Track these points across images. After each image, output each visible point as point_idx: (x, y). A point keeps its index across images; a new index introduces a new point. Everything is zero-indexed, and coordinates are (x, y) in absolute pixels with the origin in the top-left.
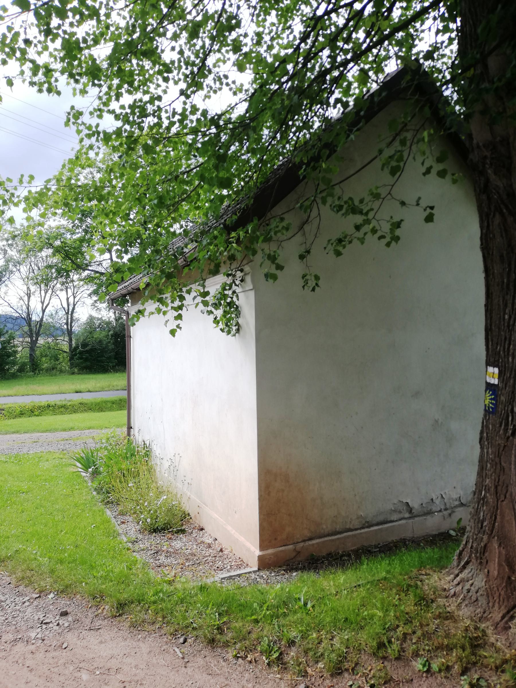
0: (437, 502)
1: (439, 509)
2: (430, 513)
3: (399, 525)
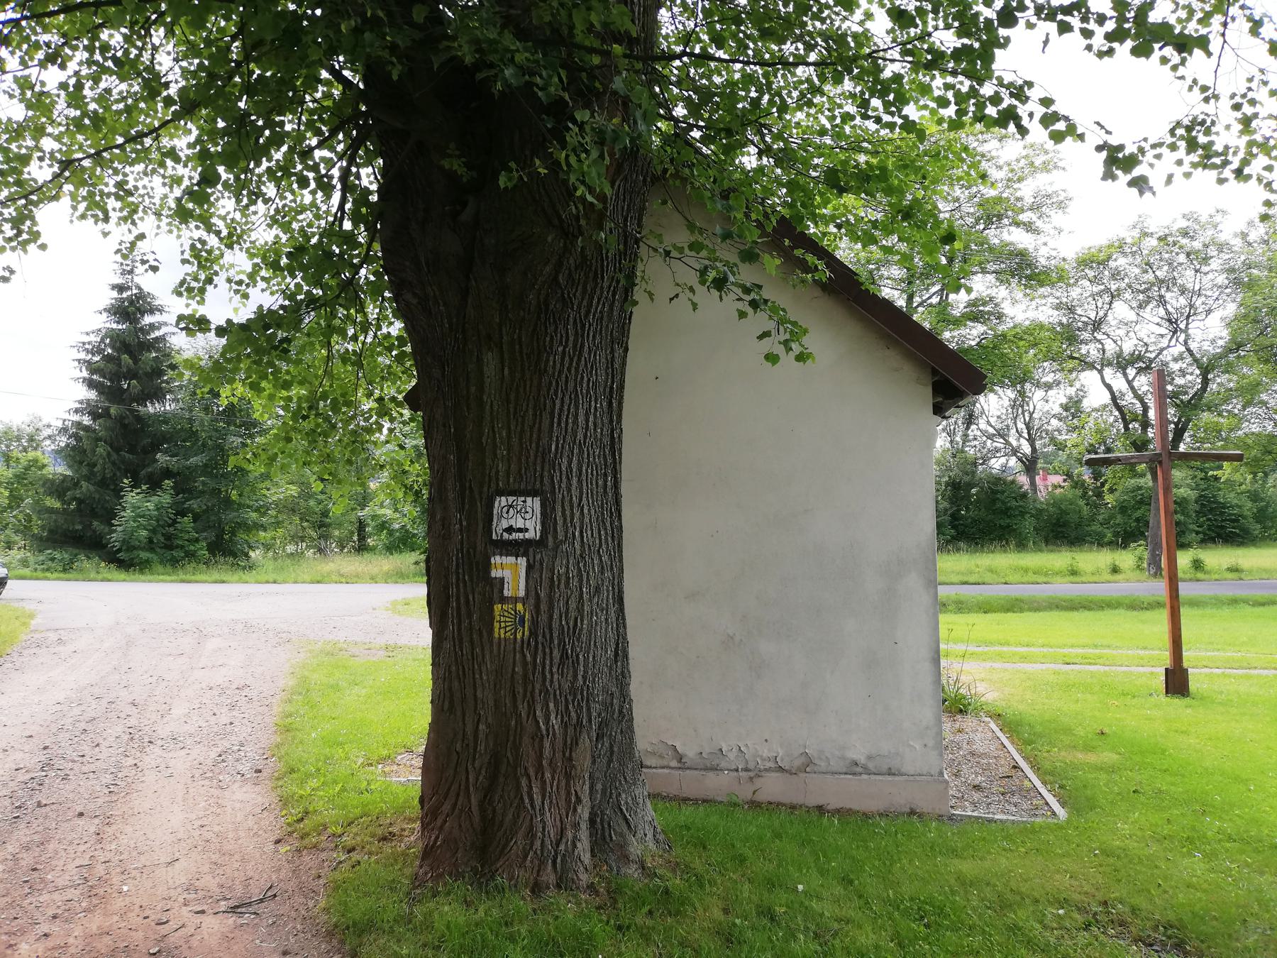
0: (732, 756)
2: (715, 769)
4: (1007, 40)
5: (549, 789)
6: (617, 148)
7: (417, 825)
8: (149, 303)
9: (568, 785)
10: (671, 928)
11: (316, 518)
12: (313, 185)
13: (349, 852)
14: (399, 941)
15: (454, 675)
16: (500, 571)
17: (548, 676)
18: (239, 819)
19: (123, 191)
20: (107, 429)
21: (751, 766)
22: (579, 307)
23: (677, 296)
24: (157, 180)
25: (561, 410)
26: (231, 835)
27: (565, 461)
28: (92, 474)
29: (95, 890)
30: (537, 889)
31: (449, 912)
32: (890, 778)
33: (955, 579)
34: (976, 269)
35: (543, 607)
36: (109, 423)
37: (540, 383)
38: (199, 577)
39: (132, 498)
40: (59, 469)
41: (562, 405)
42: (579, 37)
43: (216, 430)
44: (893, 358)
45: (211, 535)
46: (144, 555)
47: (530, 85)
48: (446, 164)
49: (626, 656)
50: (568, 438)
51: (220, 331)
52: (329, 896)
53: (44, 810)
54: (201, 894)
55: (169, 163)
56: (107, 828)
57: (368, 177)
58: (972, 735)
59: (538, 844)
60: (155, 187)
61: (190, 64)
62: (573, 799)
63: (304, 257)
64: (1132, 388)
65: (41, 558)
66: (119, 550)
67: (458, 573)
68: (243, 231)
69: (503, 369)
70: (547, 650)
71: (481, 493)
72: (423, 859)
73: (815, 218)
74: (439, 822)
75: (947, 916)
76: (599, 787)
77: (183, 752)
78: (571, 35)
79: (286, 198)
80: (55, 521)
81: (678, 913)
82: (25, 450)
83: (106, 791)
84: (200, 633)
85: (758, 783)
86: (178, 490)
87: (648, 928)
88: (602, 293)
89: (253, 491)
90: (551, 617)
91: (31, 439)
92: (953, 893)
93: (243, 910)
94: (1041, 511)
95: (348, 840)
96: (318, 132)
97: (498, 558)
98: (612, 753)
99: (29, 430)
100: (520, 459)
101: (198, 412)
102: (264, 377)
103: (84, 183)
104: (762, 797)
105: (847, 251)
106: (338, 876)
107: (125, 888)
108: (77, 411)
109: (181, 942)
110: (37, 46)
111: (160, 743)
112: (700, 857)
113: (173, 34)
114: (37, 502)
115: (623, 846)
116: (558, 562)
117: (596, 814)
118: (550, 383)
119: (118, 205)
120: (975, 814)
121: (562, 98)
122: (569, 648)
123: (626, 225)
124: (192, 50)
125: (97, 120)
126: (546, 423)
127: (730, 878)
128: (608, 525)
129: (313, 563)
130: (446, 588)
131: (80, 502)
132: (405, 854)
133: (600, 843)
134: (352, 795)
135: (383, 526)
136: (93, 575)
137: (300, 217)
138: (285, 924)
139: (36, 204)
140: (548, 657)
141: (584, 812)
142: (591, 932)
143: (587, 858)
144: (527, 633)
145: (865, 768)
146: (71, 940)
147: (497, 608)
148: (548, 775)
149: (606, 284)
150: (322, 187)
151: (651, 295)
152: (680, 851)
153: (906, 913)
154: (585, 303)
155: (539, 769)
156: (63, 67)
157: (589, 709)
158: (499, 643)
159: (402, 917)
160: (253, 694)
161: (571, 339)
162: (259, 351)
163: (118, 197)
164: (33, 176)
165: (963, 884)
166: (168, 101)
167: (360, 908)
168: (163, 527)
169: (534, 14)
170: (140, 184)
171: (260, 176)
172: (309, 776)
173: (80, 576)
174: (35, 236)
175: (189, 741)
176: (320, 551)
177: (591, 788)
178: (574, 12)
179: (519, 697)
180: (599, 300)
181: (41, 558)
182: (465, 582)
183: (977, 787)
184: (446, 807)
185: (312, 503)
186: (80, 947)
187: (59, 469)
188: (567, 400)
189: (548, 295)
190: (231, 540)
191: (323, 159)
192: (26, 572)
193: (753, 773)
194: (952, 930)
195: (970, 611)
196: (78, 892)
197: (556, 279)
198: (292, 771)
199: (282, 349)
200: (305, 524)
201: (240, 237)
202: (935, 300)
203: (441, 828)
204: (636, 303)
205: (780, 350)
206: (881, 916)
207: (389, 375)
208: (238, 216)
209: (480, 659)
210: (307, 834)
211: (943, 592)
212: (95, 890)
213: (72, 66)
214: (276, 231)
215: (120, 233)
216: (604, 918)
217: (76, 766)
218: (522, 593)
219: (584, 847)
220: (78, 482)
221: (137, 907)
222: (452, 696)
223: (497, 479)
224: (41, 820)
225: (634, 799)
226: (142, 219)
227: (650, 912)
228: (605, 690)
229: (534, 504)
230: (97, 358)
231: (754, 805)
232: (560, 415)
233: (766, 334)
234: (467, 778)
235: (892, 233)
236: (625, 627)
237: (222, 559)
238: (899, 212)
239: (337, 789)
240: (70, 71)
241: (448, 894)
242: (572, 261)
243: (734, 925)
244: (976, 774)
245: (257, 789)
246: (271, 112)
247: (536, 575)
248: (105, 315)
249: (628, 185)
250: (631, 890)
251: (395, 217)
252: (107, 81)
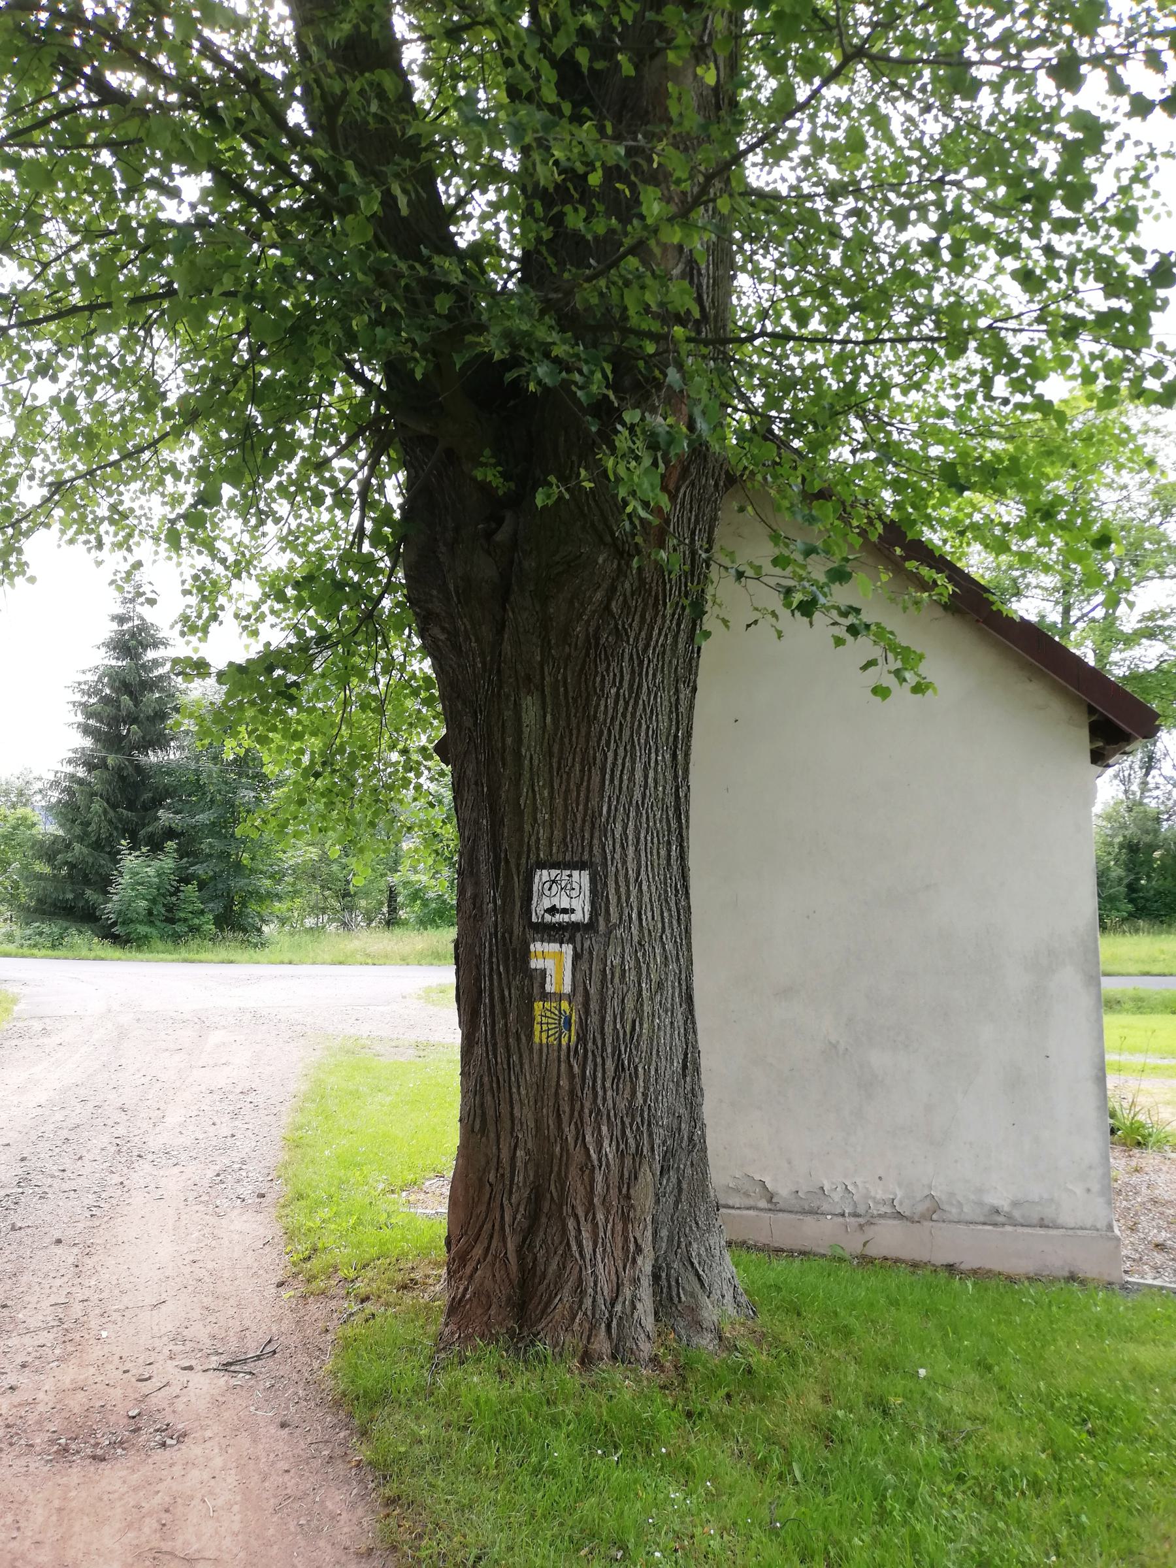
0: (836, 1196)
1: (839, 1211)
2: (814, 1212)
3: (741, 1216)
4: (1166, 301)
5: (601, 1234)
6: (672, 454)
7: (443, 1271)
8: (152, 636)
9: (625, 1229)
10: (754, 1419)
11: (339, 885)
12: (329, 501)
13: (362, 1301)
14: (417, 1418)
15: (486, 1088)
16: (541, 961)
17: (600, 1093)
18: (236, 1256)
19: (118, 516)
21: (861, 1210)
22: (636, 639)
23: (756, 622)
24: (156, 499)
25: (614, 764)
26: (226, 1274)
27: (619, 826)
28: (86, 834)
29: (70, 1333)
30: (587, 1359)
31: (478, 1383)
32: (1042, 1231)
33: (1133, 968)
34: (1152, 573)
35: (594, 1006)
36: (106, 775)
37: (588, 733)
38: (203, 956)
39: (131, 861)
40: (49, 828)
41: (615, 759)
42: (634, 321)
43: (226, 783)
44: (1036, 692)
45: (217, 906)
46: (142, 929)
47: (566, 385)
48: (479, 474)
49: (697, 1070)
50: (623, 799)
51: (221, 676)
52: (337, 1356)
53: (18, 1234)
54: (189, 1345)
55: (169, 479)
56: (86, 1260)
57: (393, 494)
58: (1153, 1176)
59: (588, 1302)
60: (152, 507)
61: (194, 366)
62: (632, 1247)
63: (316, 586)
65: (28, 932)
66: (114, 924)
67: (491, 963)
68: (252, 555)
69: (545, 717)
70: (599, 1060)
71: (518, 865)
72: (449, 1316)
73: (928, 520)
74: (468, 1270)
75: (1118, 1422)
76: (664, 1233)
77: (176, 1170)
78: (625, 317)
79: (300, 516)
80: (44, 889)
81: (763, 1399)
82: (14, 806)
83: (88, 1214)
84: (202, 1023)
85: (870, 1232)
86: (182, 853)
87: (726, 1416)
88: (664, 622)
89: (268, 854)
90: (603, 1020)
91: (21, 794)
92: (1127, 1389)
93: (237, 1368)
95: (361, 1287)
96: (335, 441)
97: (538, 944)
98: (680, 1190)
99: (18, 783)
100: (564, 824)
101: (206, 764)
102: (274, 729)
103: (75, 507)
104: (872, 1251)
105: (977, 562)
106: (349, 1332)
107: (104, 1334)
108: (70, 762)
109: (165, 1405)
110: (25, 357)
111: (150, 1157)
112: (792, 1327)
113: (176, 333)
114: (25, 867)
115: (694, 1310)
116: (611, 950)
117: (660, 1268)
118: (601, 732)
119: (112, 529)
120: (1158, 1282)
121: (606, 397)
122: (625, 1057)
123: (693, 540)
124: (197, 352)
125: (91, 437)
126: (596, 779)
127: (832, 1356)
128: (673, 905)
129: (335, 940)
130: (478, 980)
131: (72, 866)
132: (427, 1307)
133: (668, 1302)
134: (370, 1230)
135: (417, 895)
136: (84, 952)
137: (316, 538)
138: (285, 1389)
139: (27, 534)
140: (599, 1068)
141: (645, 1264)
142: (653, 1418)
143: (649, 1322)
144: (574, 1038)
145: (1009, 1216)
146: (41, 1396)
147: (538, 1006)
148: (600, 1217)
149: (669, 611)
150: (336, 501)
151: (725, 622)
152: (767, 1318)
153: (1062, 1413)
154: (643, 634)
155: (590, 1208)
156: (54, 379)
157: (650, 1135)
158: (541, 1050)
159: (423, 1388)
160: (260, 1100)
161: (627, 678)
162: (264, 698)
163: (112, 522)
164: (22, 499)
165: (1141, 1377)
166: (168, 414)
167: (373, 1373)
168: (164, 896)
169: (577, 297)
170: (135, 505)
171: (269, 492)
172: (319, 1203)
173: (70, 954)
174: (22, 566)
175: (184, 1156)
176: (344, 924)
177: (655, 1233)
178: (626, 291)
179: (565, 1118)
180: (660, 630)
181: (28, 932)
182: (500, 974)
183: (1160, 1247)
184: (478, 1252)
185: (335, 867)
186: (51, 1405)
187: (49, 828)
188: (621, 752)
189: (598, 628)
190: (241, 913)
191: (343, 470)
192: (11, 948)
193: (865, 1220)
194: (1126, 1441)
195: (1153, 1010)
196: (51, 1336)
197: (607, 608)
198: (300, 1197)
199: (287, 693)
200: (327, 893)
201: (249, 563)
202: (1099, 613)
203: (471, 1277)
204: (707, 635)
205: (890, 681)
206: (1029, 1417)
207: (419, 721)
208: (246, 538)
209: (517, 1069)
210: (315, 1277)
211: (1109, 986)
212: (70, 1333)
213: (64, 377)
214: (289, 555)
215: (116, 561)
216: (670, 1400)
217: (56, 1183)
218: (567, 989)
220: (70, 844)
221: (116, 1357)
222: (484, 1114)
223: (538, 849)
224: (15, 1246)
225: (709, 1250)
226: (138, 544)
227: (728, 1396)
228: (671, 1111)
229: (582, 879)
230: (93, 700)
231: (866, 1260)
232: (612, 771)
233: (872, 663)
234: (502, 1217)
235: (1029, 536)
236: (695, 1032)
237: (231, 935)
238: (1037, 511)
239: (352, 1222)
240: (62, 384)
241: (479, 1360)
242: (627, 585)
243: (836, 1417)
244: (1160, 1228)
245: (260, 1217)
246: (280, 420)
247: (585, 967)
248: (104, 649)
249: (696, 492)
250: (704, 1366)
251: (422, 536)
252: (102, 392)
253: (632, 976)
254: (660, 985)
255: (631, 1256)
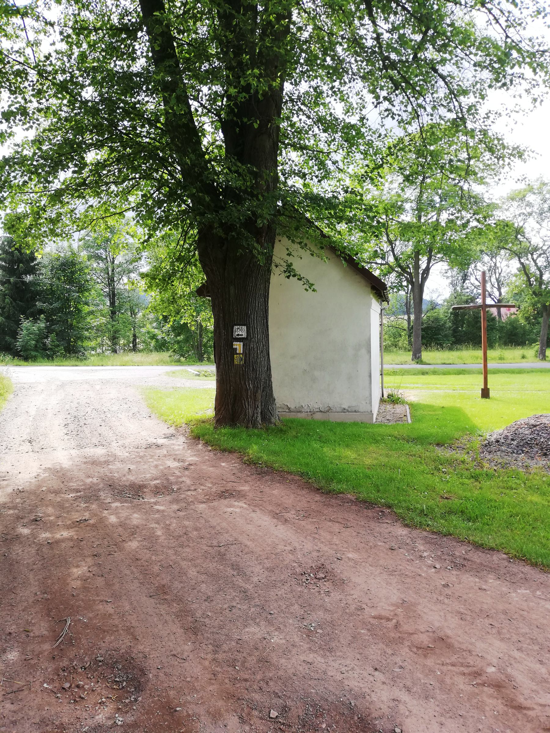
0: (305, 408)
2: (300, 412)
20: (8, 289)
33: (439, 362)
38: (64, 364)
39: (26, 324)
46: (33, 353)
64: (536, 264)
66: (21, 351)
94: (502, 327)
115: (270, 419)
133: (264, 418)
141: (259, 410)
184: (223, 409)
193: (313, 413)
219: (259, 419)
228: (264, 379)
229: (244, 328)
253: (256, 349)
254: (262, 352)
255: (256, 408)
